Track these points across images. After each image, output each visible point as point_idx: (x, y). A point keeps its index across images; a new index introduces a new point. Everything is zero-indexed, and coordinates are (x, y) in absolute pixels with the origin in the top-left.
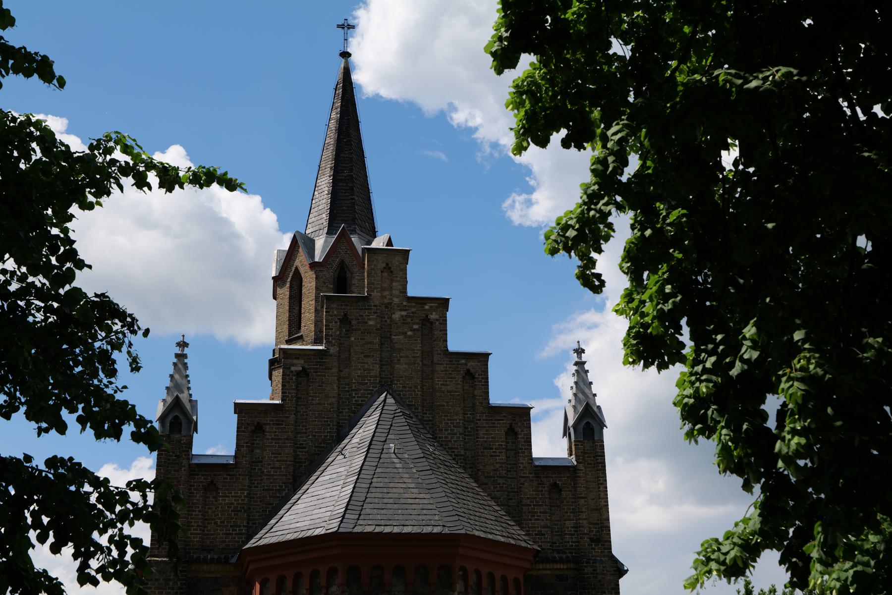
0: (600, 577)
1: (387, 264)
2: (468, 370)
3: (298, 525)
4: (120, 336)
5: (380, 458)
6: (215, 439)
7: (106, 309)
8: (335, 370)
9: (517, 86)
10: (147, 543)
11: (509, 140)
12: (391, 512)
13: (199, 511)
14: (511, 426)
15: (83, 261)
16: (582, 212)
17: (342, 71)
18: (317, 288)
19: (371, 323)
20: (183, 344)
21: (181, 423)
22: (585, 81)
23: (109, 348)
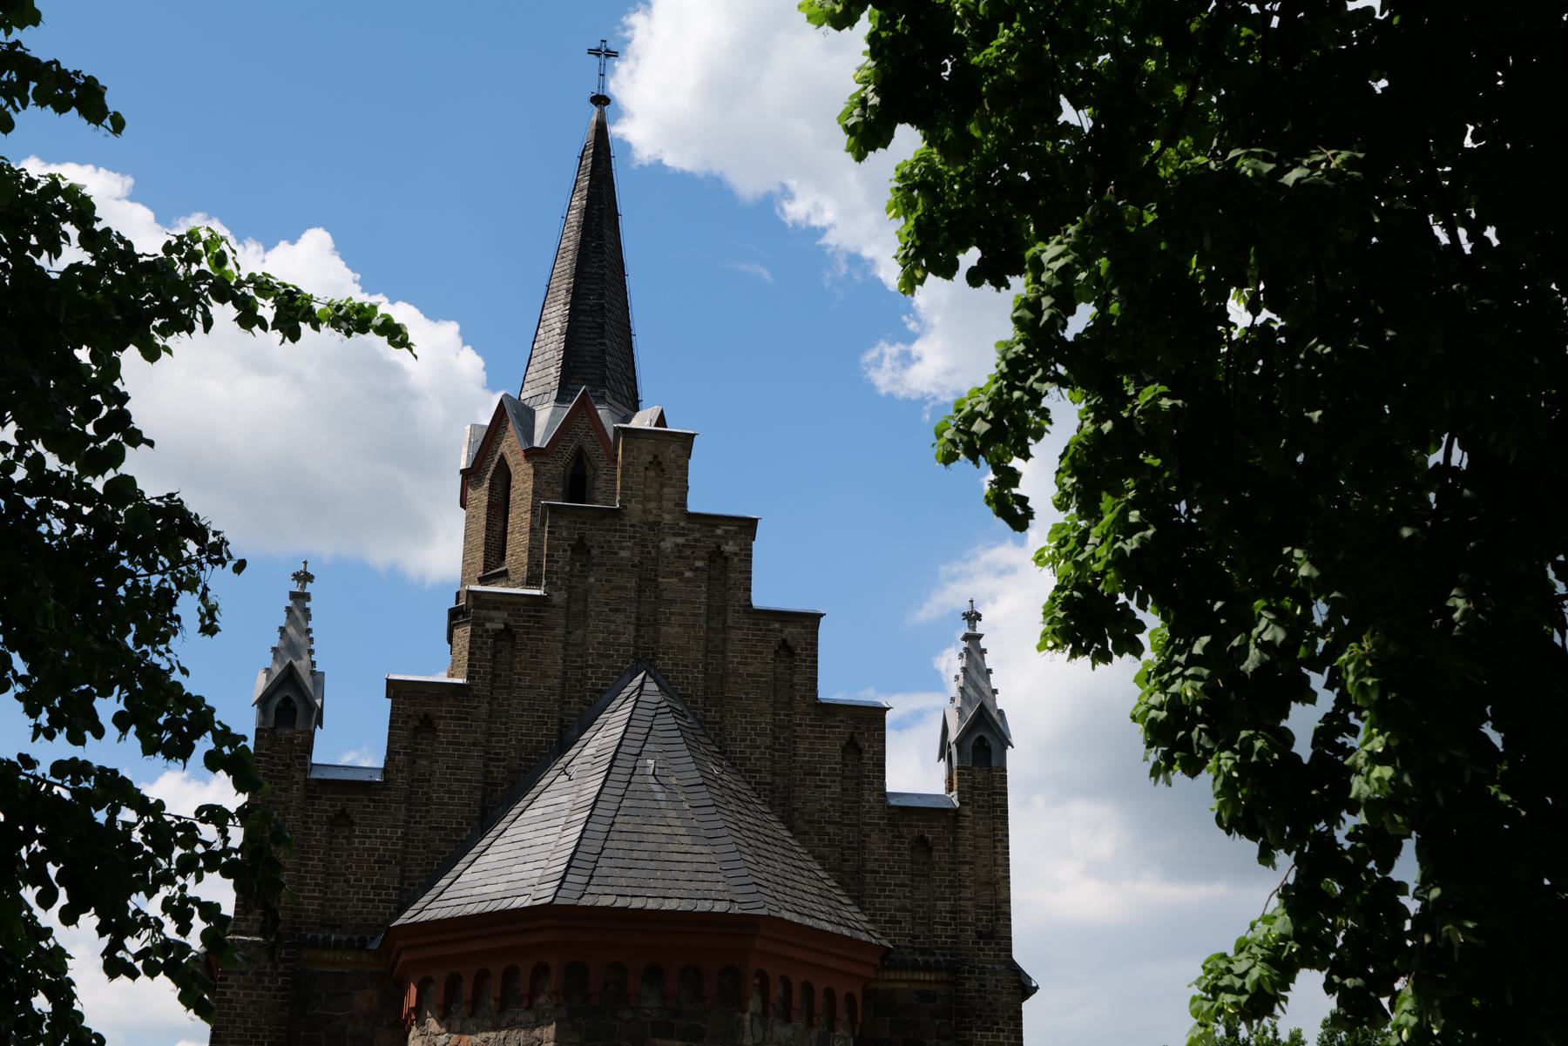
0: (990, 998)
1: (656, 457)
2: (784, 641)
3: (485, 889)
4: (194, 567)
5: (629, 782)
6: (352, 740)
7: (173, 525)
8: (559, 631)
9: (903, 177)
10: (228, 909)
11: (891, 274)
12: (643, 874)
13: (320, 860)
14: (852, 738)
15: (140, 432)
16: (999, 392)
17: (593, 127)
18: (535, 492)
19: (624, 554)
20: (304, 577)
21: (295, 711)
22: (1016, 167)
23: (174, 586)
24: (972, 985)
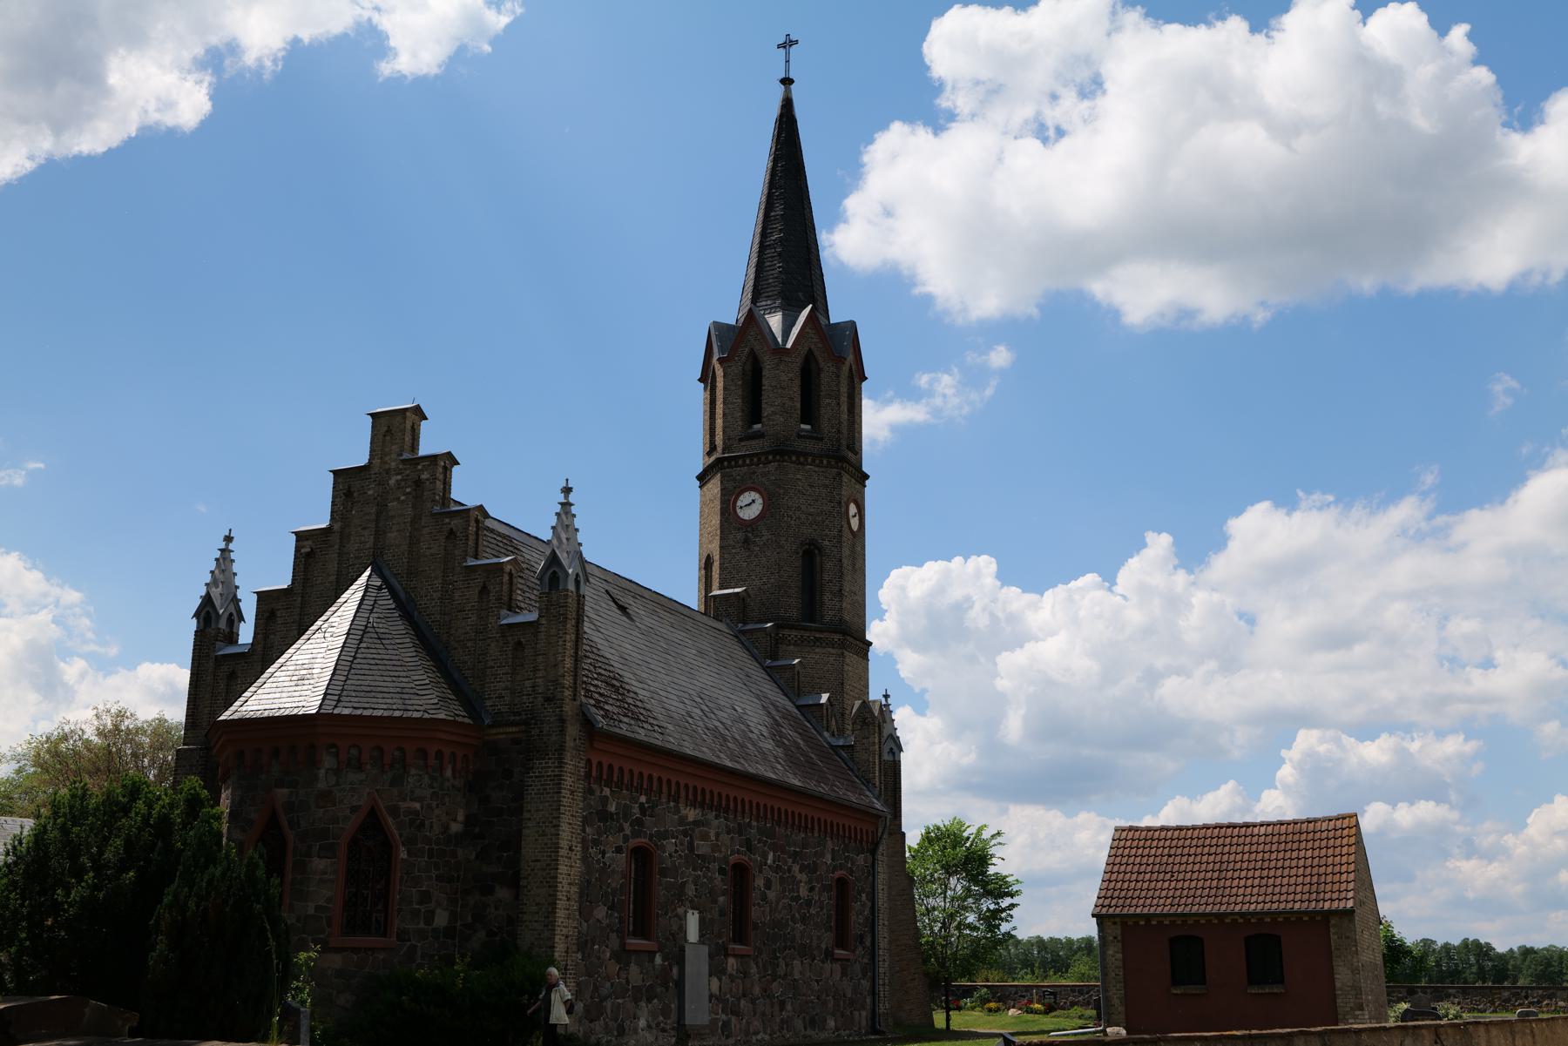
24: (535, 732)
